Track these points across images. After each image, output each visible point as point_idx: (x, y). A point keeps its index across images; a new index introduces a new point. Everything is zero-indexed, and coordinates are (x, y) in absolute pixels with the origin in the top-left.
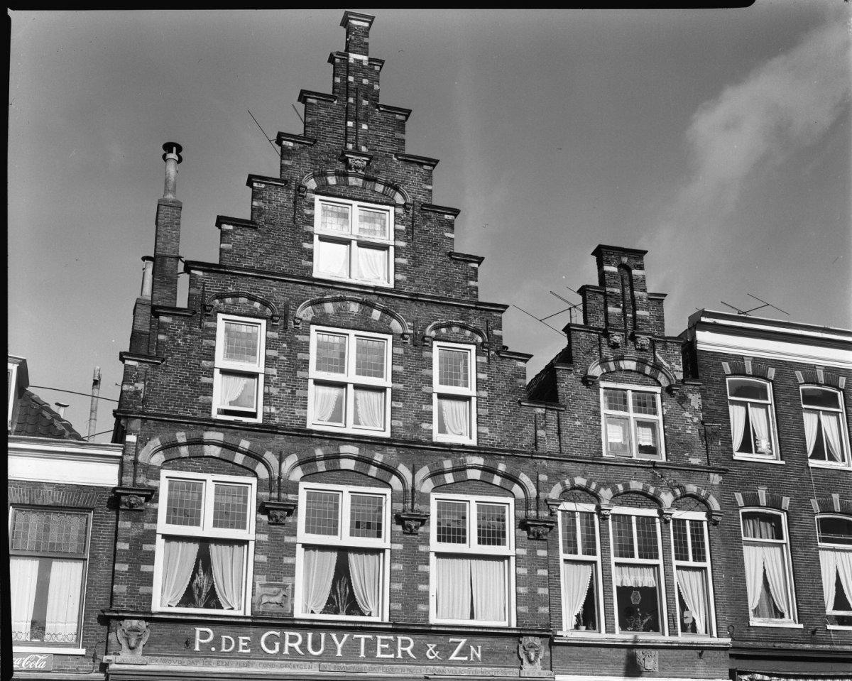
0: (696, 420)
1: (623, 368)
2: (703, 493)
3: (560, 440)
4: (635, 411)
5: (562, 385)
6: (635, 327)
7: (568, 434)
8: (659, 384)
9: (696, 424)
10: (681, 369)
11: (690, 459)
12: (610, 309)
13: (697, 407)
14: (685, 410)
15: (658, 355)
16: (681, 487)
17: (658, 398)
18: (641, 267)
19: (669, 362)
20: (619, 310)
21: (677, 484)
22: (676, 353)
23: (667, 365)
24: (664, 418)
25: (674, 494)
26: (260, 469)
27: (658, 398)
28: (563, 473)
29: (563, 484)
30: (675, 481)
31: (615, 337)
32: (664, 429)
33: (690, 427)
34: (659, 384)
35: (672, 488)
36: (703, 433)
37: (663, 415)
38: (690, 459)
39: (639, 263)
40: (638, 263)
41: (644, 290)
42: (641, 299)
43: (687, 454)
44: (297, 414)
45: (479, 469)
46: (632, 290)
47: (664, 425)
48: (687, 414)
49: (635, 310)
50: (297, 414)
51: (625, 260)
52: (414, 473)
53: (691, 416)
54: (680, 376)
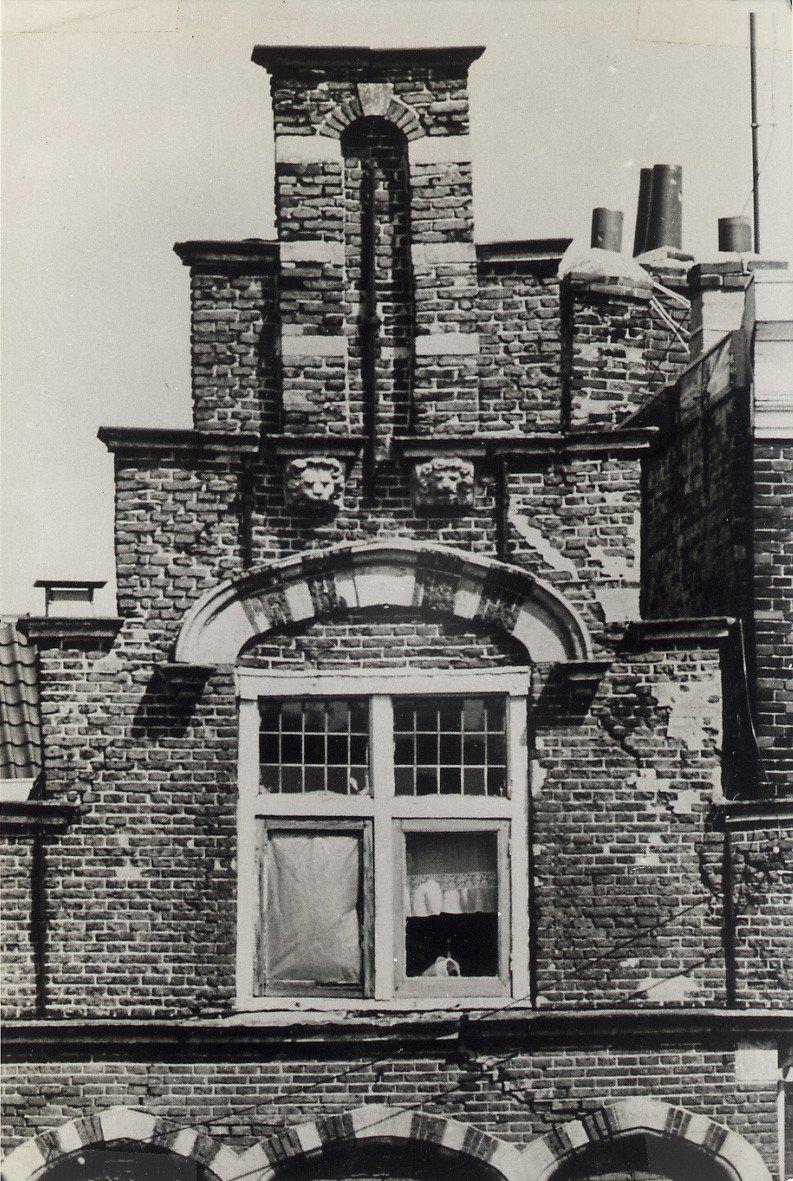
0: (687, 801)
1: (351, 603)
2: (697, 1130)
3: (40, 958)
4: (403, 786)
5: (65, 707)
6: (409, 412)
7: (83, 924)
8: (517, 654)
9: (685, 819)
10: (634, 574)
11: (644, 984)
12: (295, 343)
13: (696, 743)
14: (640, 761)
15: (519, 522)
16: (591, 1112)
17: (517, 717)
18: (454, 125)
20: (339, 346)
21: (572, 1102)
22: (614, 499)
23: (561, 564)
24: (531, 811)
25: (557, 1142)
26: (530, 629)
27: (517, 717)
28: (50, 1096)
29: (52, 1143)
30: (563, 1090)
31: (309, 475)
32: (532, 859)
33: (655, 839)
34: (517, 654)
35: (544, 1118)
36: (715, 855)
37: (531, 799)
38: (644, 984)
40: (438, 106)
41: (461, 235)
42: (442, 278)
43: (632, 962)
44: (539, 422)
46: (406, 235)
47: (532, 840)
48: (647, 781)
49: (408, 329)
50: (539, 422)
51: (377, 98)
53: (664, 785)
54: (624, 607)
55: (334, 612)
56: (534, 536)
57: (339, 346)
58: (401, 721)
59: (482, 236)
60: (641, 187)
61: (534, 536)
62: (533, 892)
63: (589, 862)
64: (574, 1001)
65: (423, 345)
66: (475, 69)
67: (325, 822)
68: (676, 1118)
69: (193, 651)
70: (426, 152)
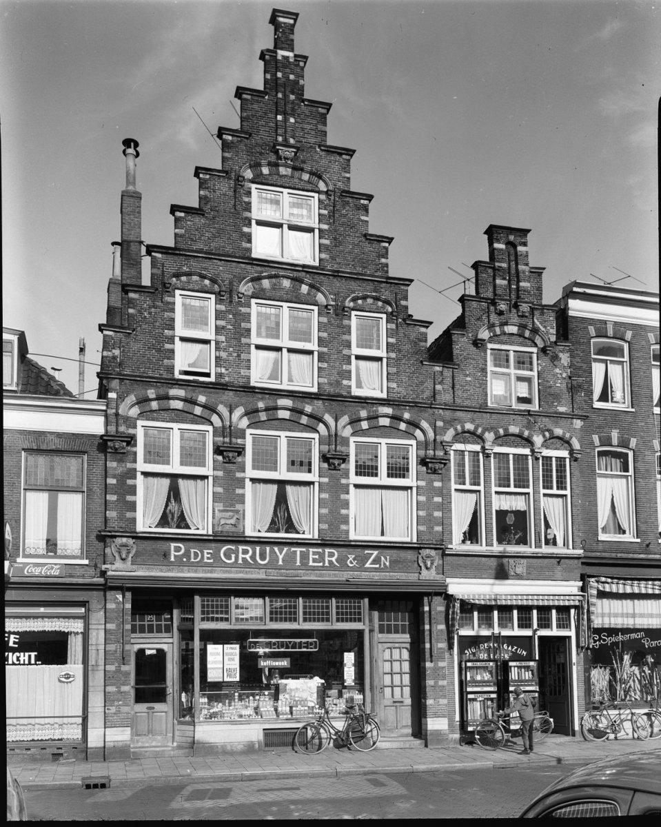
2: (568, 435)
4: (515, 368)
5: (457, 347)
6: (518, 297)
8: (536, 345)
9: (565, 378)
11: (558, 408)
12: (498, 281)
14: (556, 366)
15: (536, 320)
17: (535, 356)
18: (525, 244)
19: (545, 327)
20: (505, 282)
22: (551, 318)
25: (544, 436)
27: (535, 356)
29: (456, 429)
32: (539, 383)
33: (559, 381)
34: (536, 345)
36: (569, 386)
38: (558, 408)
39: (523, 240)
45: (388, 417)
46: (517, 264)
47: (538, 380)
48: (557, 370)
49: (518, 281)
52: (336, 421)
54: (553, 339)
55: (504, 333)
56: (538, 323)
57: (505, 282)
58: (556, 461)
59: (531, 265)
60: (56, 526)
61: (538, 323)
62: (539, 389)
63: (548, 384)
64: (546, 408)
65: (522, 284)
66: (529, 235)
67: (556, 795)
68: (564, 433)
69: (480, 336)
70: (520, 248)
